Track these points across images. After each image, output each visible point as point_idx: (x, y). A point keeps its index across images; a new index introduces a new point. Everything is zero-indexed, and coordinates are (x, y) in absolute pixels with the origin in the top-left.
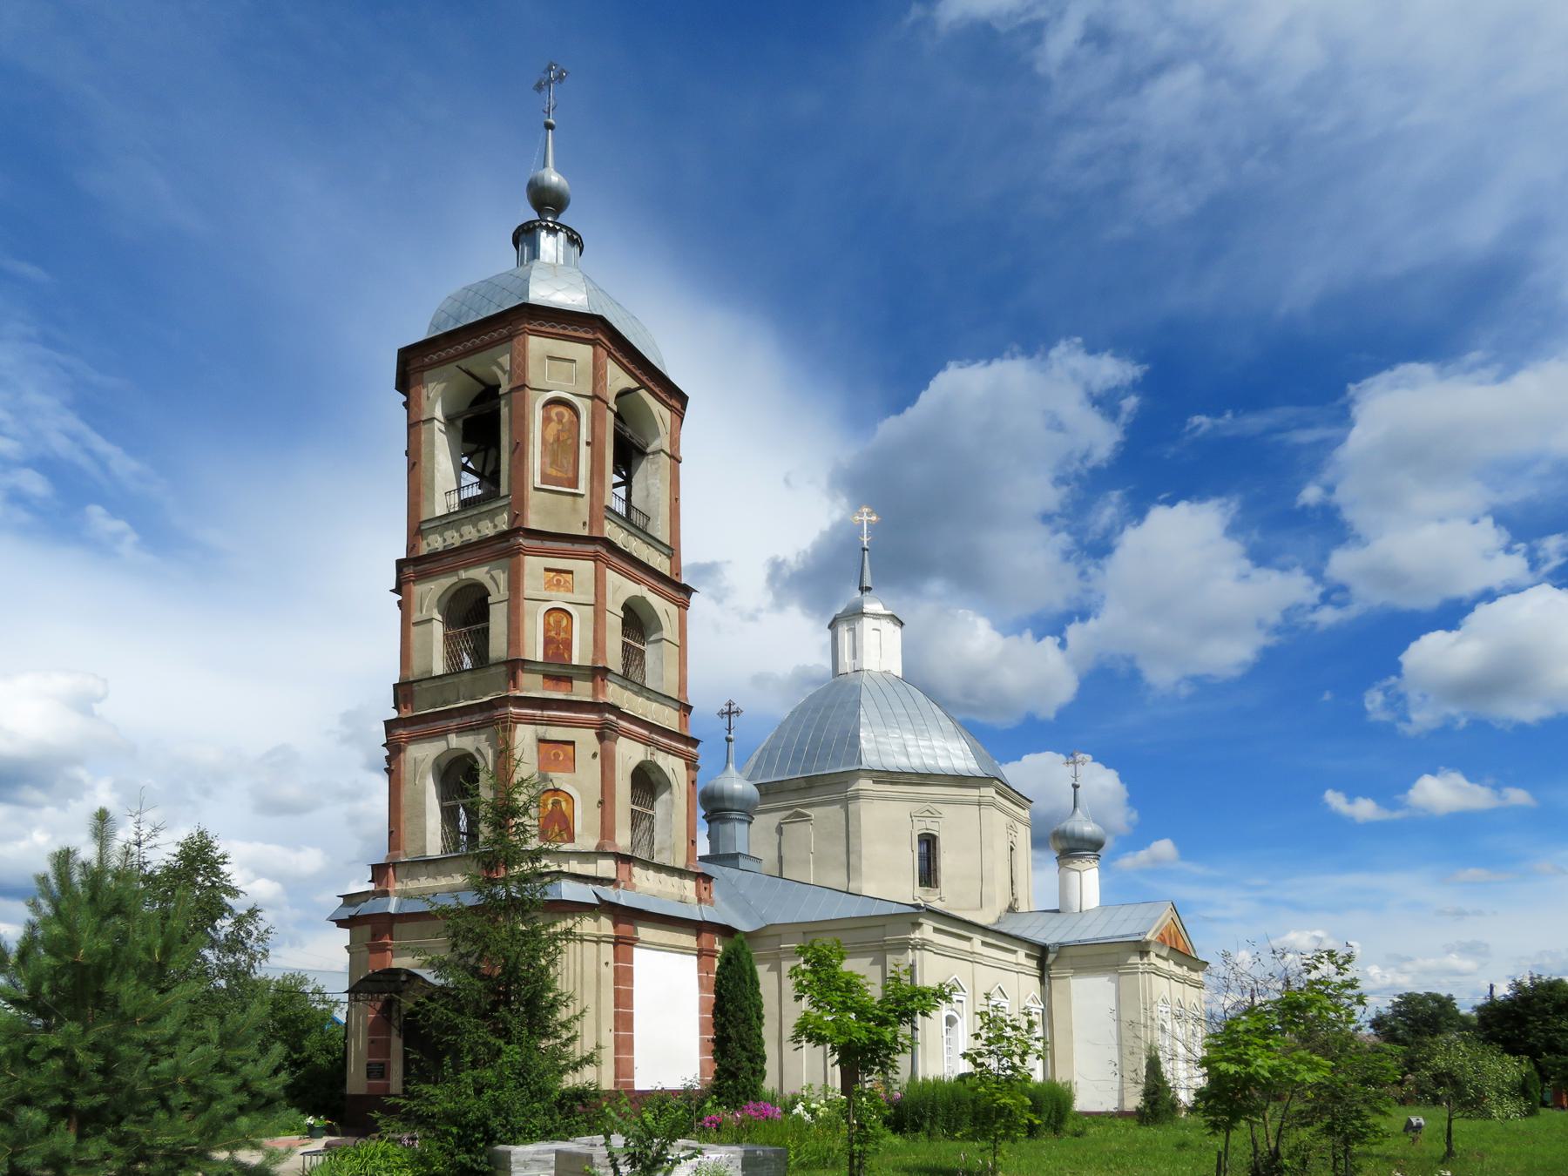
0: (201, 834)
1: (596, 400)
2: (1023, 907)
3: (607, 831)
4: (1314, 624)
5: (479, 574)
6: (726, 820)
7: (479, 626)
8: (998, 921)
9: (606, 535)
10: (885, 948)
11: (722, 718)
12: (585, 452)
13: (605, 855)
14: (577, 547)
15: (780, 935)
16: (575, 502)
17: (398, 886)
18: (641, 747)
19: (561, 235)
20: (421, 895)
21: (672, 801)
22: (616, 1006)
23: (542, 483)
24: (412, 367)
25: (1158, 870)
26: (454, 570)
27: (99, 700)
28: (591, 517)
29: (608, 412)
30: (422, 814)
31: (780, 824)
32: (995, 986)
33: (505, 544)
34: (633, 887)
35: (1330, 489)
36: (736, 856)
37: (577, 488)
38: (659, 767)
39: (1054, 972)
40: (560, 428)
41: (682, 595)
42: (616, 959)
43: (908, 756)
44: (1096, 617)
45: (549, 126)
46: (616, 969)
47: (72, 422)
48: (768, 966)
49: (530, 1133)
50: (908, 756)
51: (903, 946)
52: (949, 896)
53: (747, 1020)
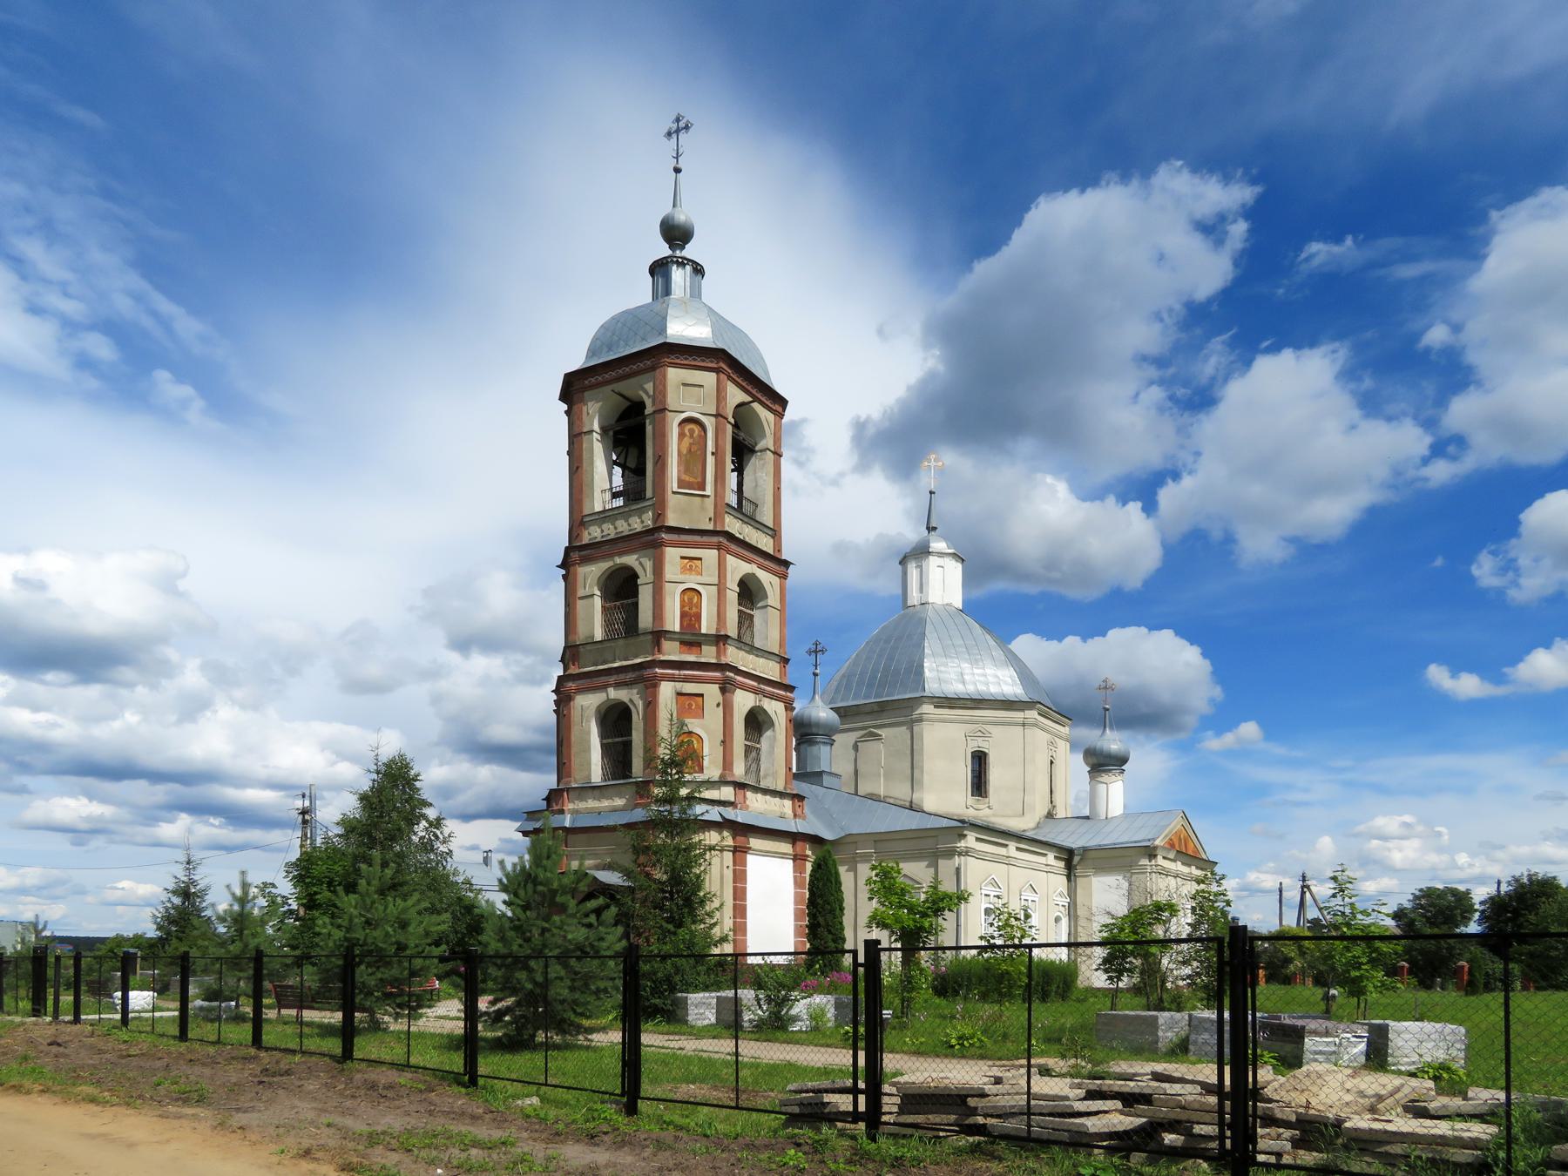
1: (720, 418)
2: (1060, 813)
3: (727, 763)
4: (1426, 479)
5: (630, 560)
6: (812, 743)
7: (629, 601)
8: (1038, 826)
9: (727, 529)
12: (710, 460)
13: (727, 783)
14: (705, 539)
16: (703, 502)
17: (571, 806)
20: (590, 812)
21: (775, 737)
22: (735, 899)
23: (679, 487)
25: (1242, 753)
26: (611, 556)
27: (184, 575)
28: (715, 513)
30: (588, 750)
31: (856, 742)
34: (747, 807)
35: (1457, 328)
36: (821, 773)
37: (704, 490)
39: (1079, 872)
40: (691, 441)
41: (783, 568)
42: (735, 863)
43: (964, 683)
44: (1190, 473)
46: (734, 871)
47: (135, 281)
48: (846, 867)
49: (696, 986)
50: (964, 683)
51: (951, 853)
52: (998, 809)
53: (832, 911)
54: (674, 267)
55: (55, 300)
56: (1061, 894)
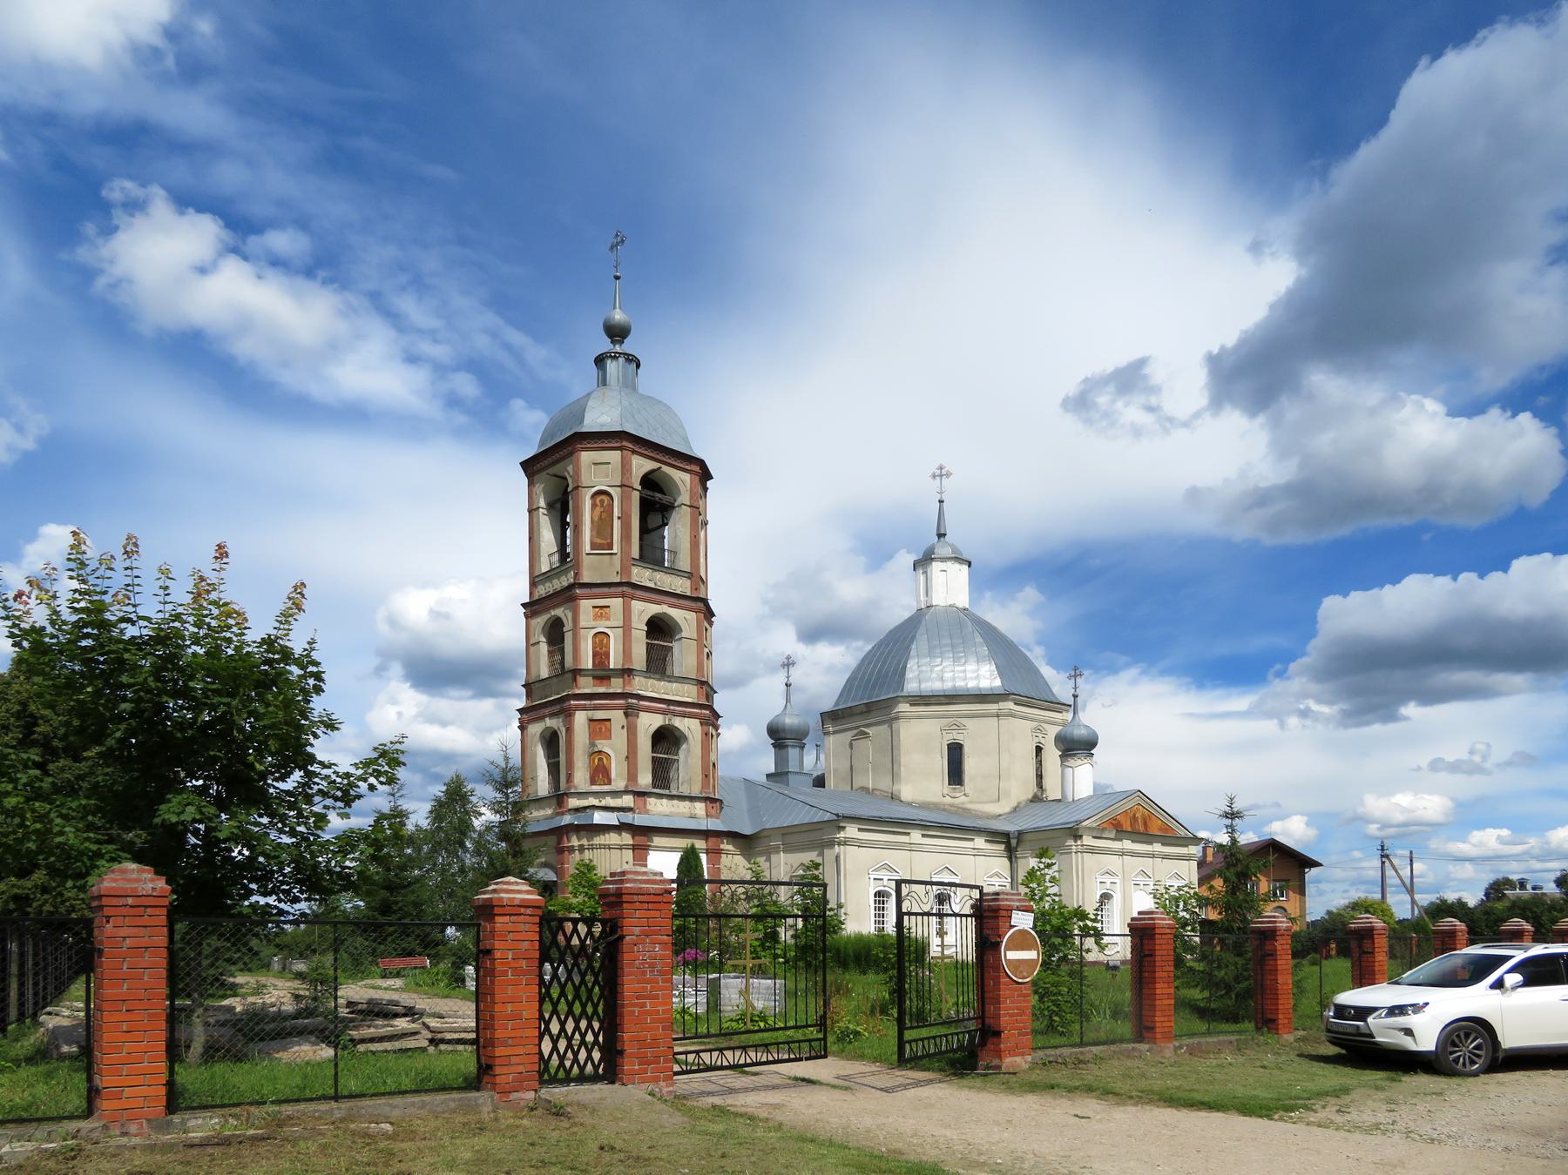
0: (457, 776)
3: (632, 775)
5: (559, 612)
14: (612, 590)
23: (592, 549)
26: (547, 610)
45: (617, 278)
47: (491, 319)
51: (831, 844)
54: (609, 362)
55: (426, 348)
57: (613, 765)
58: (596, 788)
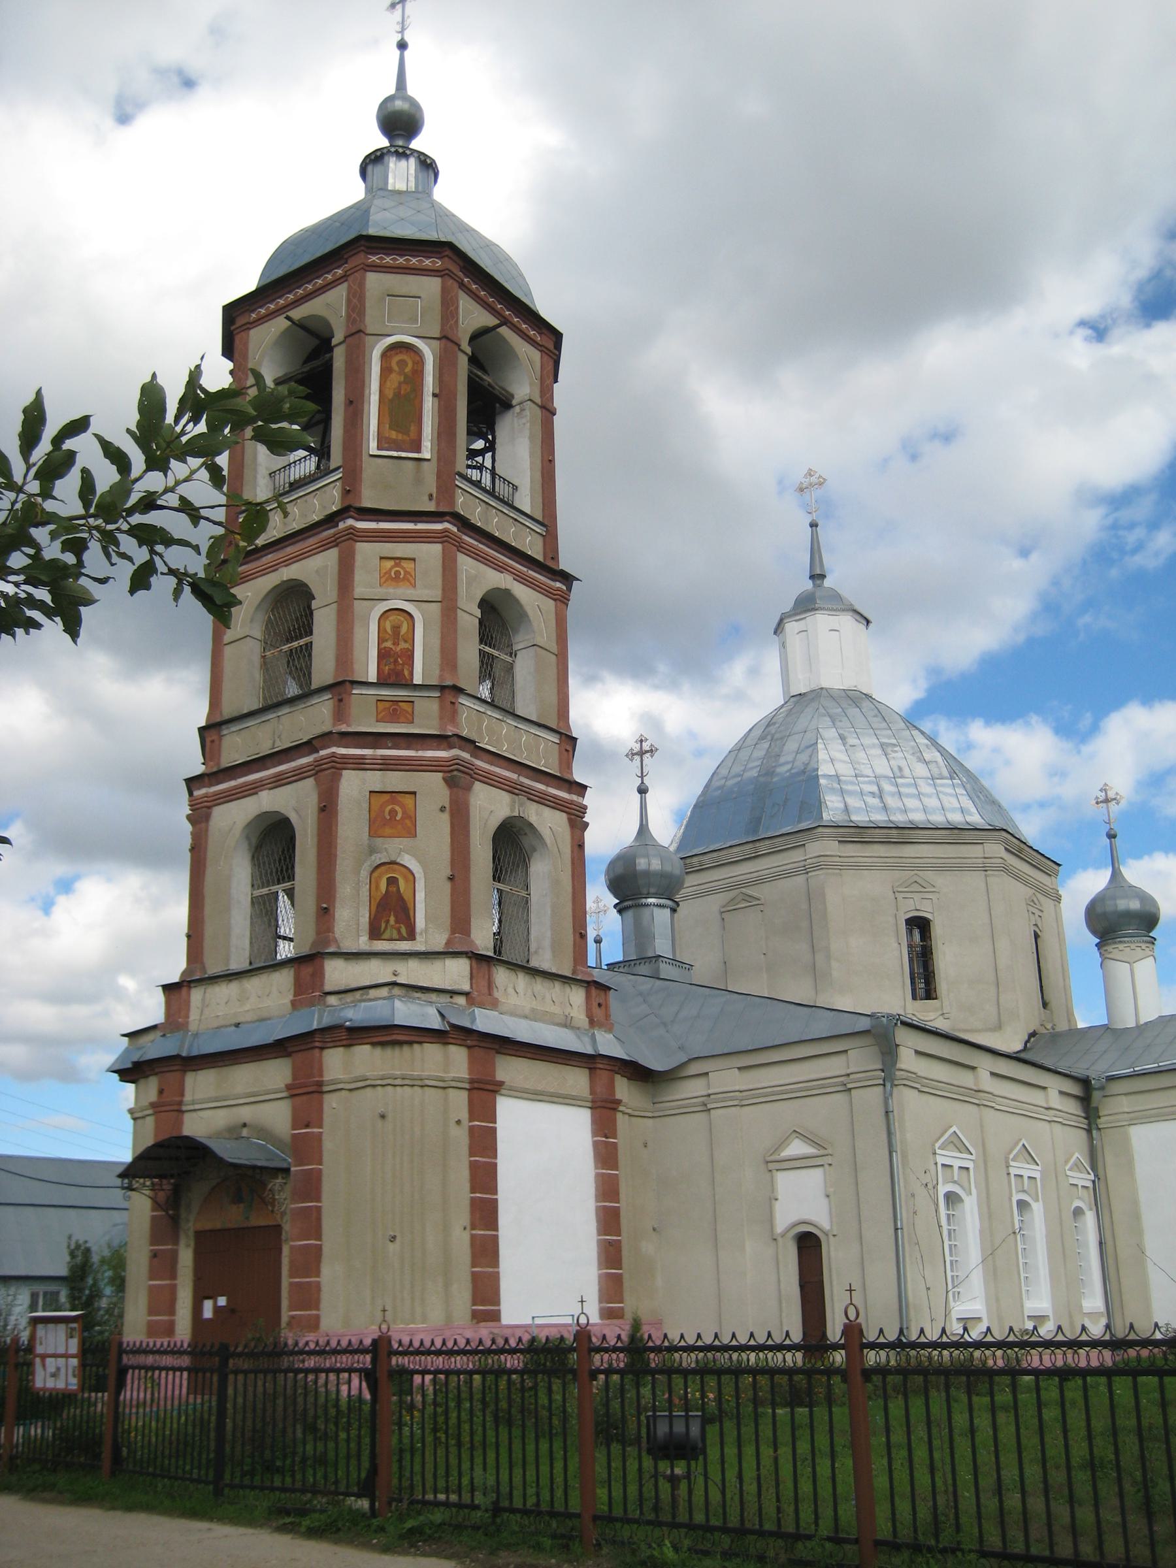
3: (460, 922)
7: (302, 642)
10: (849, 1086)
11: (632, 760)
12: (429, 405)
15: (707, 1074)
16: (418, 471)
18: (505, 797)
19: (412, 161)
23: (379, 448)
24: (237, 325)
29: (461, 355)
32: (1016, 1144)
33: (332, 531)
37: (419, 450)
38: (531, 825)
56: (1077, 1166)
57: (420, 896)
58: (381, 946)
